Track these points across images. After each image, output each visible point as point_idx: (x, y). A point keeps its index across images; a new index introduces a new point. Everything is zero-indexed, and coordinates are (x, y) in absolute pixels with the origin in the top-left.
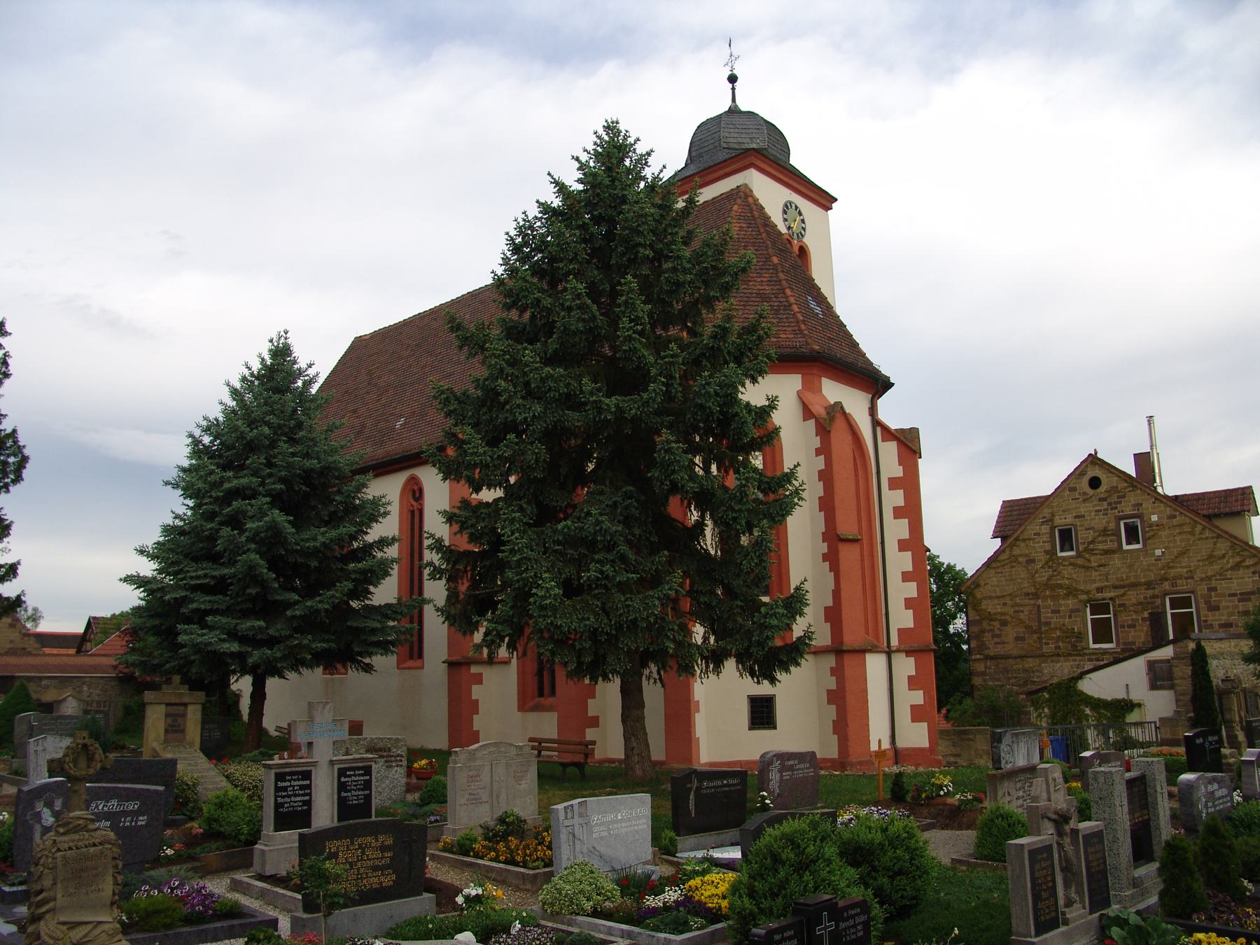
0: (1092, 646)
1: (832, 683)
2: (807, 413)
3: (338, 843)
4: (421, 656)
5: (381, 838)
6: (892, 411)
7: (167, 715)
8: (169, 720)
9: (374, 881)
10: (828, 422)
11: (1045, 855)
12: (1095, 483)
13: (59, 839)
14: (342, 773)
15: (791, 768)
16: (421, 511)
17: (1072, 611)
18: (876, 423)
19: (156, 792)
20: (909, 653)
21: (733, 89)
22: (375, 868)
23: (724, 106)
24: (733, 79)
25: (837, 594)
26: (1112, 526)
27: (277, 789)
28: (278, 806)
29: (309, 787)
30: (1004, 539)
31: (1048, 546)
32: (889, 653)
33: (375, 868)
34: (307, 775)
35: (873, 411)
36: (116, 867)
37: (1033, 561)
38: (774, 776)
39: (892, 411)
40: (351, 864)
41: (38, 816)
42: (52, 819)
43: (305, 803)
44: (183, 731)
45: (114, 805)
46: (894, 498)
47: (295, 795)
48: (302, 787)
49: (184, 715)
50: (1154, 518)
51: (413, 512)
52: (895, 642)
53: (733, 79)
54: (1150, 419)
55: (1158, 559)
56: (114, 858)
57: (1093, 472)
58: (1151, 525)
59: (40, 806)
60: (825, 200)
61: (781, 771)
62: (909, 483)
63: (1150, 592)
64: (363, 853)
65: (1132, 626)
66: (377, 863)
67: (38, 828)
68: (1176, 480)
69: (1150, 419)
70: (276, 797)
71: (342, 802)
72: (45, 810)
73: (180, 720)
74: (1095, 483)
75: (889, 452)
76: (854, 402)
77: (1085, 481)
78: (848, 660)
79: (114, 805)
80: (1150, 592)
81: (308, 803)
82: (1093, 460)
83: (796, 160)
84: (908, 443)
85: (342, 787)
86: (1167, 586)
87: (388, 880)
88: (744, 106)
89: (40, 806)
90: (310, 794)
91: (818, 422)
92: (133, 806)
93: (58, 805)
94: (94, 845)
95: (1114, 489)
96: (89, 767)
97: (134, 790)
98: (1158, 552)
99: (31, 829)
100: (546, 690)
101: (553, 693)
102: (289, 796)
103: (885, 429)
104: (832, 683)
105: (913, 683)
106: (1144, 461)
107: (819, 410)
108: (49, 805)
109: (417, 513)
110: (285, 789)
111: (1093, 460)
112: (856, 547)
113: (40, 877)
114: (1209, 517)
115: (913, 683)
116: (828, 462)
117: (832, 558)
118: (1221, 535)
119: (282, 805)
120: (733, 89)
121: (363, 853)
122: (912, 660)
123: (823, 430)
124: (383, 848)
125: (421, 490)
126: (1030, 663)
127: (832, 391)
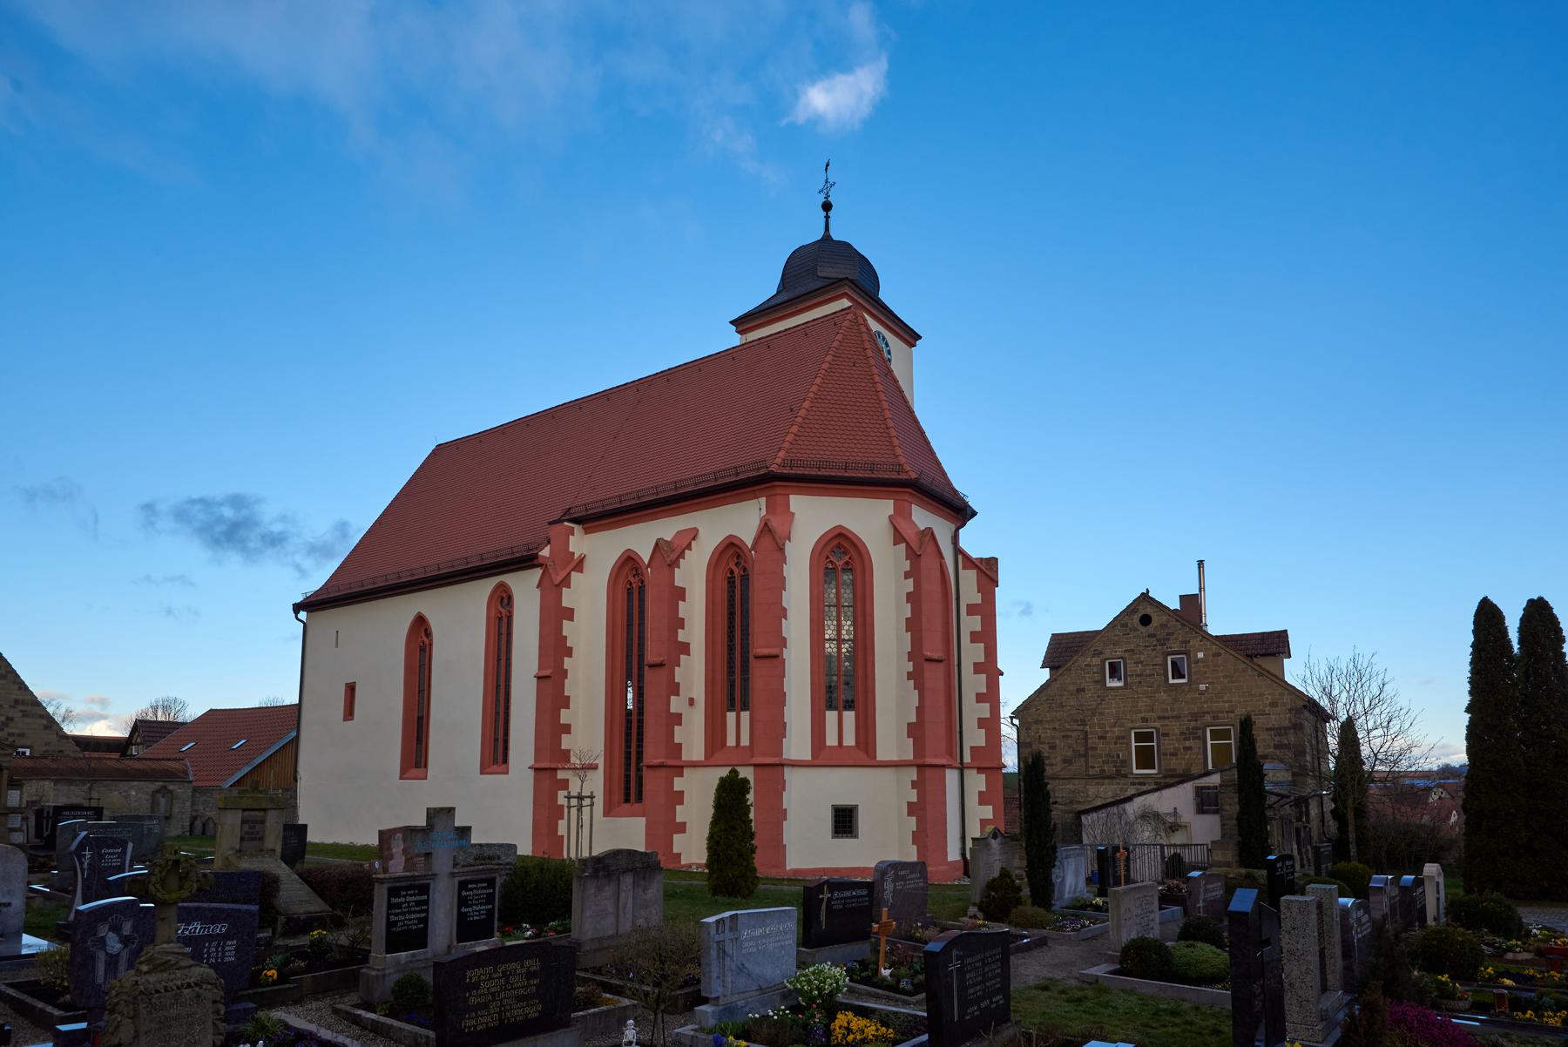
0: (1136, 771)
1: (913, 796)
2: (898, 538)
3: (479, 971)
4: (505, 761)
5: (527, 963)
6: (974, 540)
7: (243, 822)
8: (246, 828)
9: (518, 1013)
10: (919, 550)
11: (163, 801)
12: (1146, 620)
13: (142, 980)
14: (463, 886)
15: (903, 879)
16: (510, 618)
17: (1118, 738)
18: (958, 551)
19: (248, 912)
20: (980, 770)
21: (827, 217)
22: (520, 999)
23: (819, 235)
24: (827, 207)
25: (920, 710)
26: (1159, 660)
27: (390, 906)
28: (390, 924)
29: (426, 902)
30: (1052, 669)
31: (1097, 677)
32: (962, 769)
33: (520, 999)
34: (425, 890)
35: (955, 539)
36: (217, 1012)
37: (1083, 690)
38: (889, 886)
39: (974, 540)
40: (493, 995)
41: (102, 942)
42: (119, 946)
43: (421, 920)
44: (261, 839)
45: (196, 928)
46: (971, 624)
47: (410, 913)
48: (418, 903)
49: (263, 822)
50: (1201, 655)
51: (500, 619)
52: (967, 759)
53: (827, 207)
54: (351, 689)
55: (1202, 693)
56: (214, 1002)
57: (1143, 610)
58: (1197, 661)
59: (103, 930)
60: (911, 337)
61: (894, 881)
62: (986, 610)
63: (1193, 724)
64: (507, 982)
65: (1174, 754)
66: (522, 992)
67: (102, 956)
68: (1218, 623)
69: (351, 689)
70: (388, 915)
71: (462, 918)
72: (111, 934)
73: (258, 827)
74: (1146, 620)
75: (969, 578)
76: (941, 528)
77: (1136, 618)
78: (929, 772)
79: (196, 928)
80: (1193, 724)
81: (425, 921)
82: (1145, 597)
83: (882, 296)
84: (987, 571)
85: (463, 902)
86: (1208, 718)
87: (533, 1012)
88: (836, 235)
89: (103, 930)
90: (427, 911)
91: (908, 545)
92: (220, 929)
93: (127, 928)
94: (189, 986)
95: (1164, 626)
96: (181, 888)
97: (222, 910)
98: (1202, 687)
99: (92, 958)
100: (633, 797)
101: (640, 798)
102: (403, 914)
103: (966, 557)
104: (913, 796)
105: (983, 799)
106: (1192, 604)
107: (908, 533)
108: (116, 929)
109: (505, 620)
110: (399, 906)
111: (1145, 597)
112: (941, 667)
113: (117, 1027)
114: (1250, 656)
115: (983, 799)
116: (917, 584)
117: (916, 676)
118: (1264, 673)
119: (395, 924)
120: (827, 217)
121: (507, 982)
122: (983, 776)
123: (913, 555)
124: (530, 975)
125: (510, 598)
126: (1077, 785)
127: (922, 518)
